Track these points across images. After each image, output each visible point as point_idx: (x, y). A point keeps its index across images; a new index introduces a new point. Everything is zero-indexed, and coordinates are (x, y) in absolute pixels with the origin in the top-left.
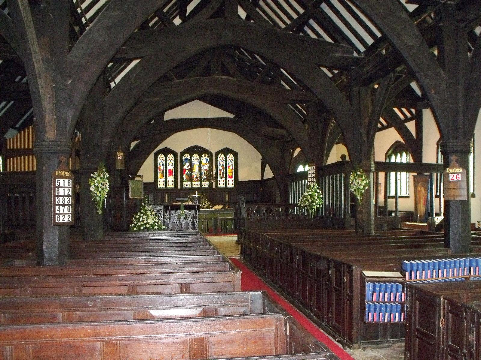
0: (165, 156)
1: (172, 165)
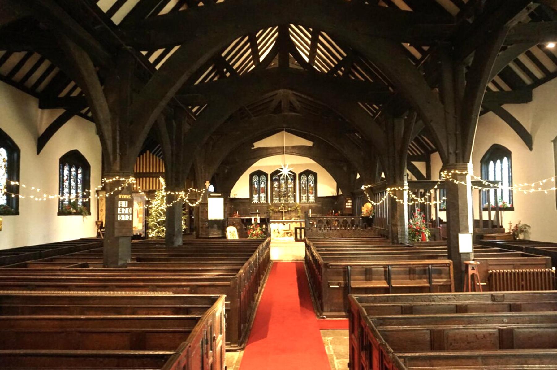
0: (258, 177)
1: (264, 184)
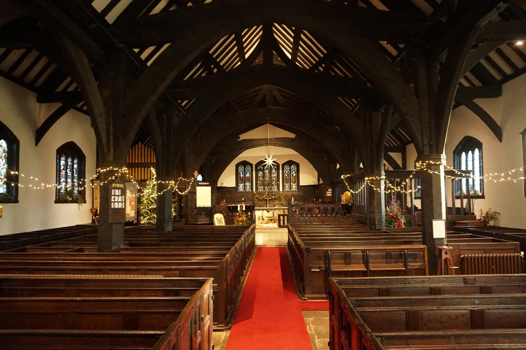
1: (249, 173)
